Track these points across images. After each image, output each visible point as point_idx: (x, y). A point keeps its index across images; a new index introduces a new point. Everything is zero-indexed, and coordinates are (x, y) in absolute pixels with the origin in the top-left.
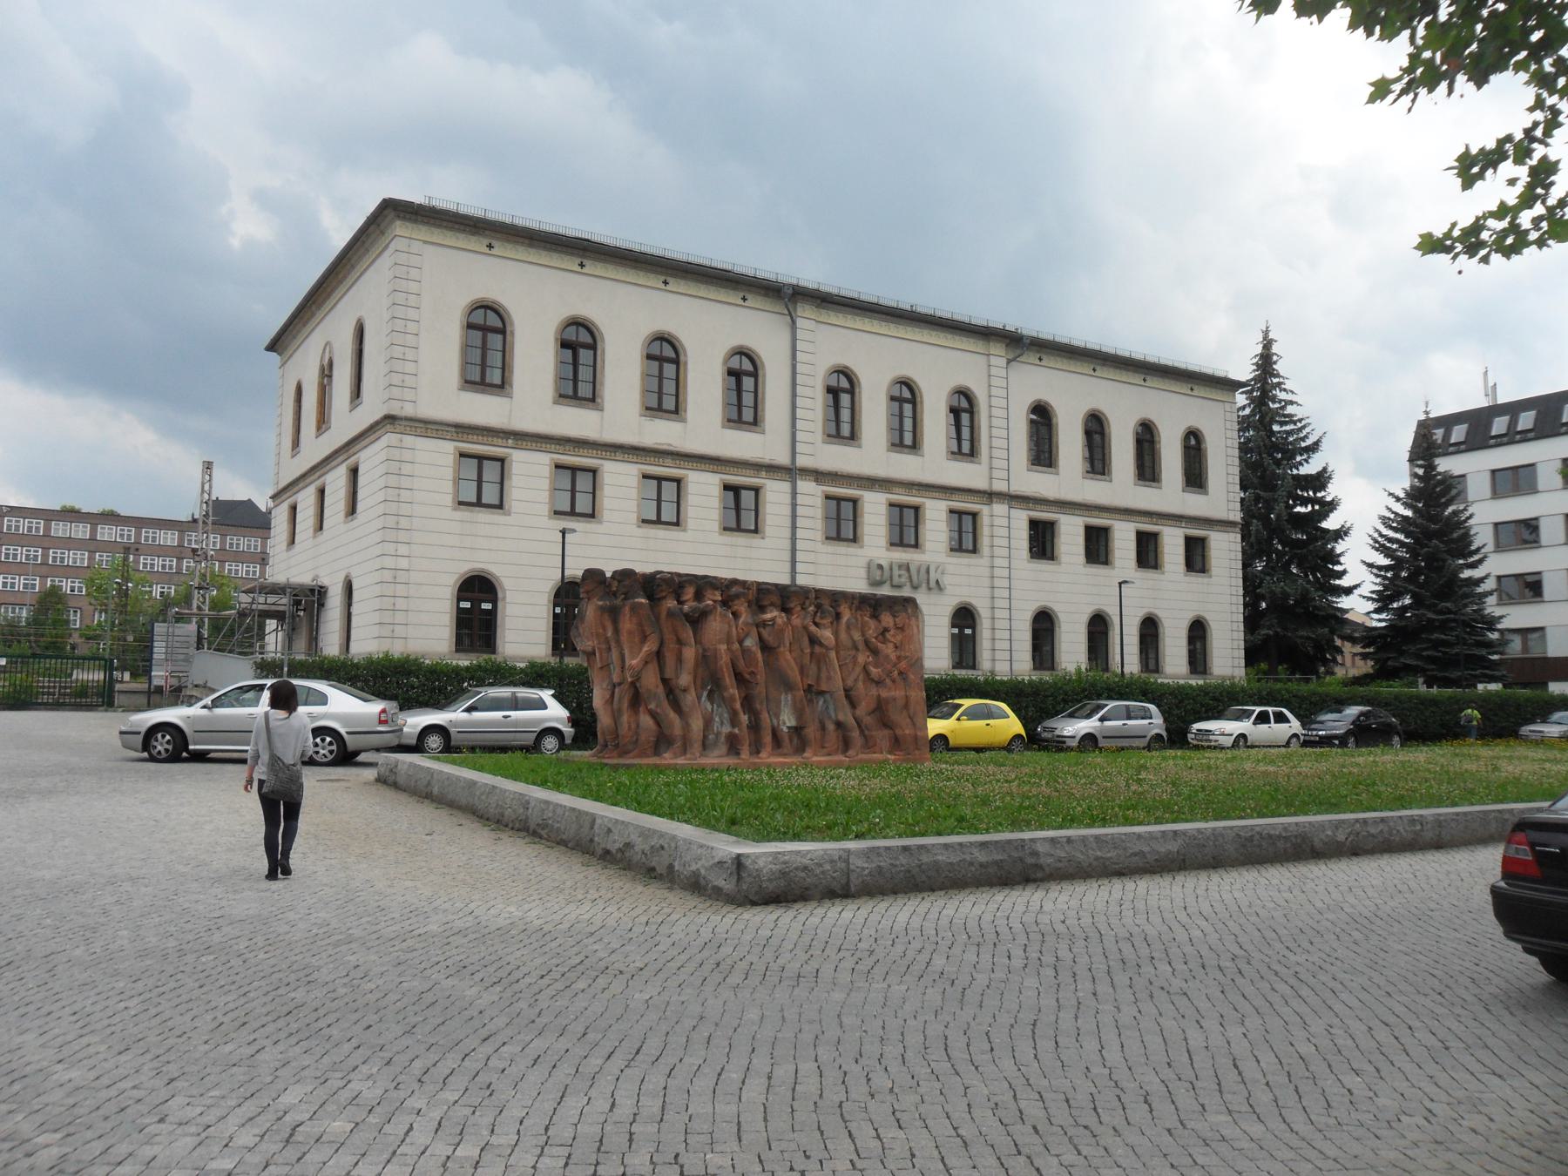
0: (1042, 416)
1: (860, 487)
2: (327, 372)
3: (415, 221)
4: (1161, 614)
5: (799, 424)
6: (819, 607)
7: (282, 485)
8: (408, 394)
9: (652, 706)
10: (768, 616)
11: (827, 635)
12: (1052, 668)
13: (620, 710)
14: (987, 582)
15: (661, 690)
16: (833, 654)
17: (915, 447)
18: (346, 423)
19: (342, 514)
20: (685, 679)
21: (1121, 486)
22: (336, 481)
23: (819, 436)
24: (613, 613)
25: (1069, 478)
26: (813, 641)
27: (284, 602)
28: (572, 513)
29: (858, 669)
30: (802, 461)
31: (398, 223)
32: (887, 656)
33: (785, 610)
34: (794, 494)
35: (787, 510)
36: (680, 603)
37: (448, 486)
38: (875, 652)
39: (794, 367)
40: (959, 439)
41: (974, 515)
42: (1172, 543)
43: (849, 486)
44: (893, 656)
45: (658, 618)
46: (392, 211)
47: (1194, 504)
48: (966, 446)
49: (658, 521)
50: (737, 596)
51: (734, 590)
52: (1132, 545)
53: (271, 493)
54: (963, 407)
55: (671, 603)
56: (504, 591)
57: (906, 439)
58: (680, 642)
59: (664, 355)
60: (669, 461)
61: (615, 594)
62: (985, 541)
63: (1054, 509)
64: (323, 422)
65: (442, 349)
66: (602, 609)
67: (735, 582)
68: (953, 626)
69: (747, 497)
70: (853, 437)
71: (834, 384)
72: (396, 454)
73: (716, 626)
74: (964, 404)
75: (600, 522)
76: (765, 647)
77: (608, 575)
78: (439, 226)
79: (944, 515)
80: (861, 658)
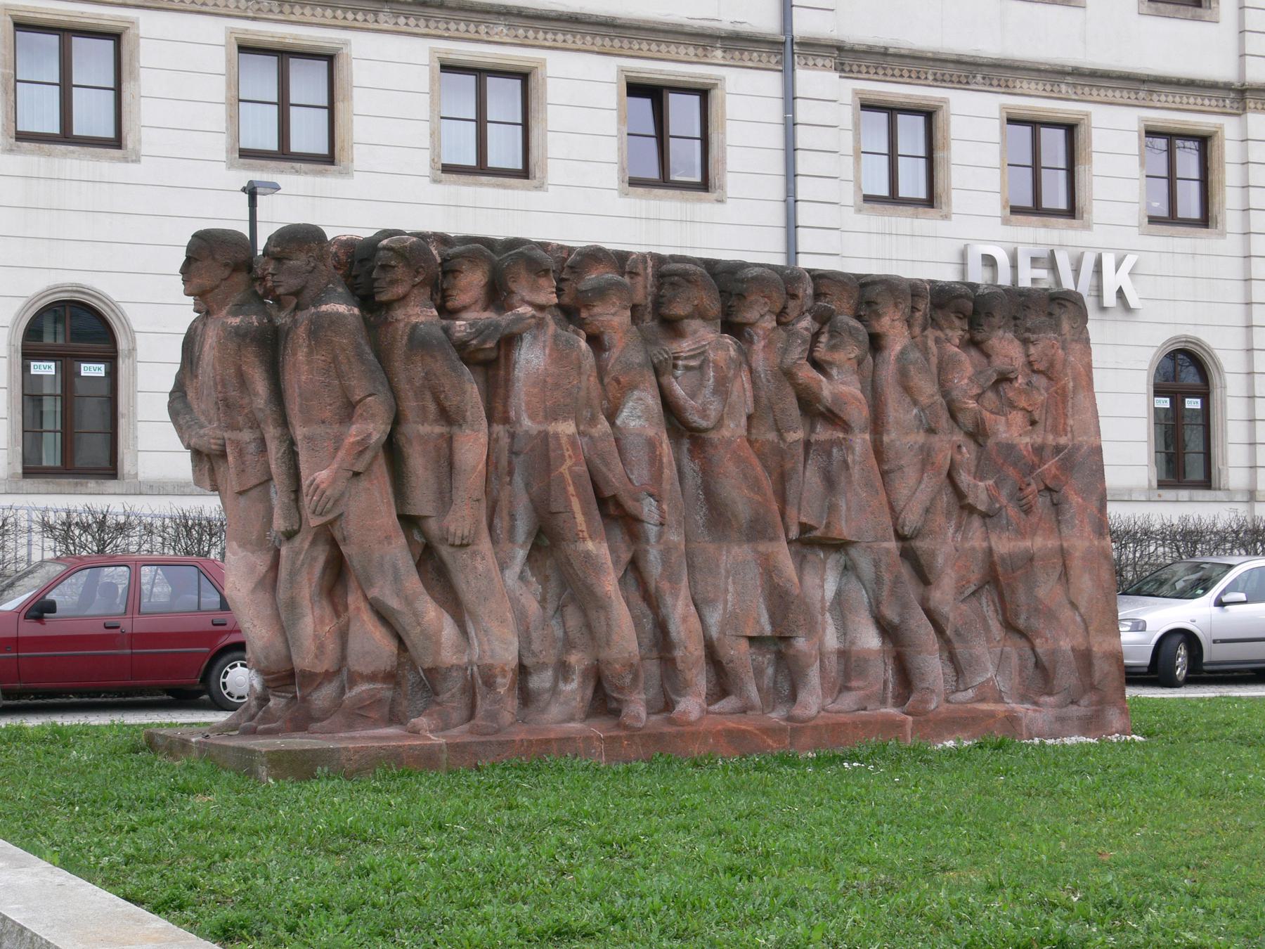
1: (940, 81)
6: (824, 319)
10: (685, 346)
13: (293, 604)
14: (1235, 292)
15: (399, 552)
20: (463, 518)
33: (733, 327)
34: (790, 98)
35: (775, 137)
36: (447, 312)
41: (1203, 142)
43: (898, 79)
45: (383, 357)
50: (601, 292)
51: (594, 277)
55: (419, 314)
56: (131, 334)
58: (448, 416)
60: (500, 30)
62: (1229, 199)
66: (240, 335)
67: (594, 256)
68: (1158, 392)
69: (682, 111)
75: (347, 173)
79: (1133, 142)
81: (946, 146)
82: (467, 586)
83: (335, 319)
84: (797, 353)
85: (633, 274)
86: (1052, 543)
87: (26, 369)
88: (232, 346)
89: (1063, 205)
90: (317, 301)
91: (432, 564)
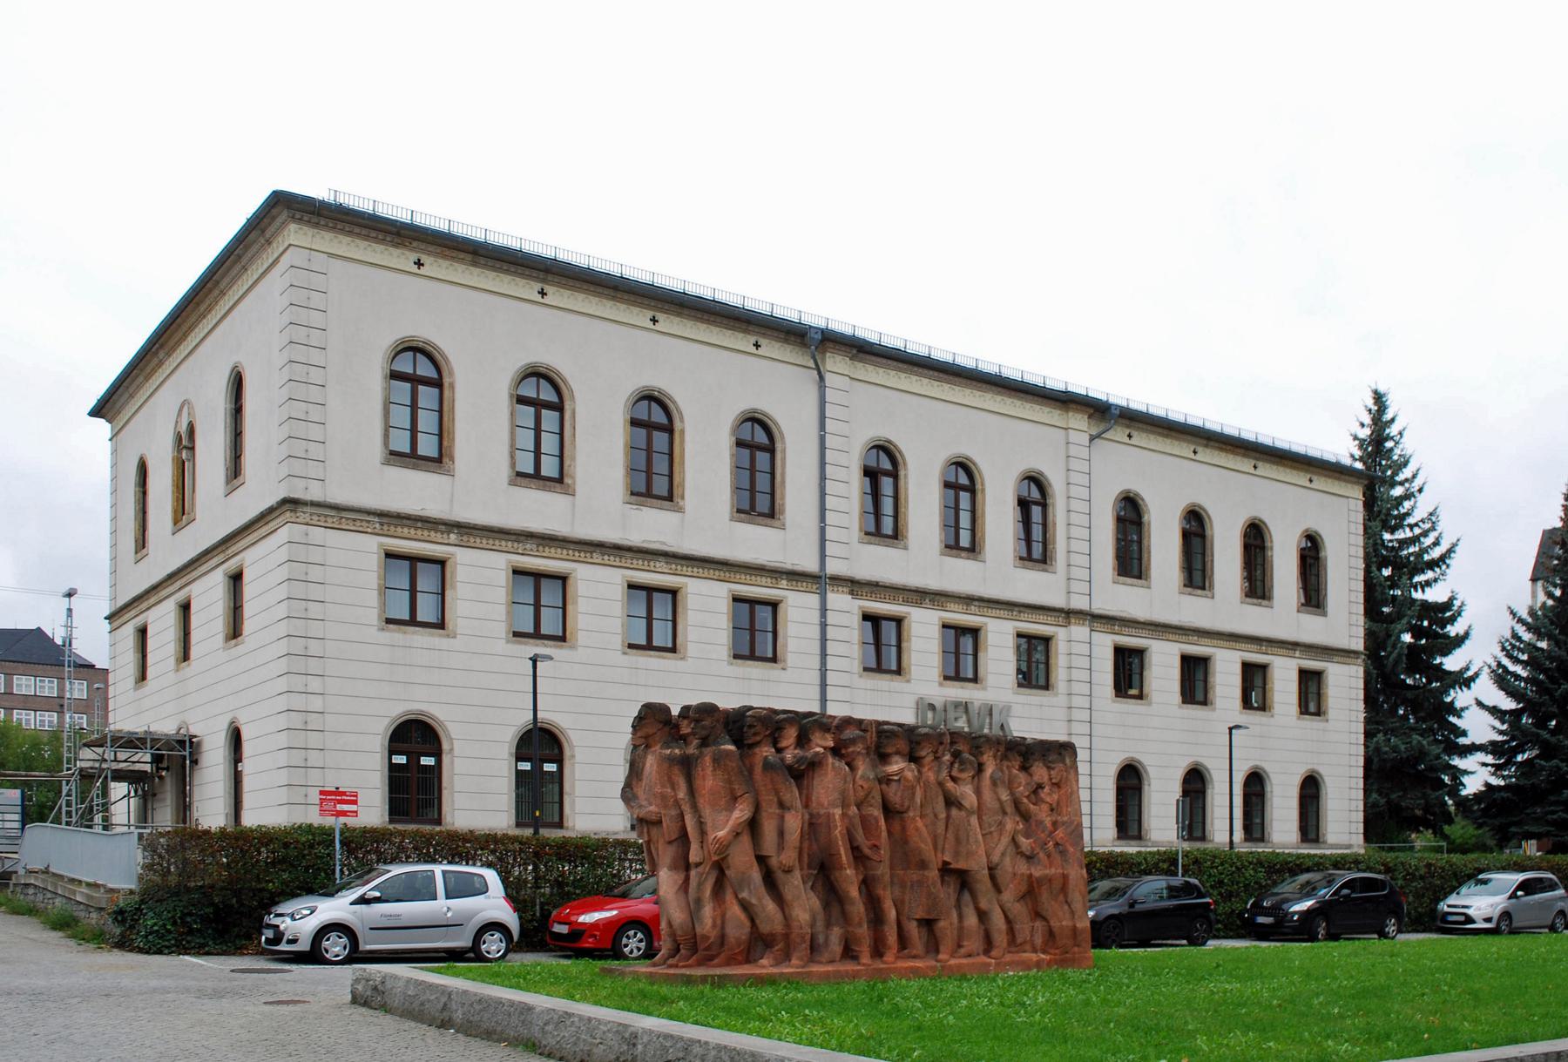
0: (1130, 514)
1: (906, 602)
2: (186, 443)
3: (316, 225)
4: (1269, 767)
5: (829, 516)
6: (956, 755)
7: (120, 603)
8: (314, 470)
9: (744, 895)
11: (966, 792)
12: (1139, 837)
13: (699, 901)
15: (756, 875)
16: (974, 820)
17: (974, 550)
18: (218, 511)
19: (221, 637)
21: (1224, 604)
22: (209, 593)
23: (855, 533)
24: (687, 765)
25: (1161, 593)
26: (951, 802)
27: (142, 760)
28: (537, 635)
29: (1005, 840)
30: (833, 567)
31: (293, 226)
32: (1040, 823)
33: (913, 758)
34: (824, 610)
36: (779, 750)
37: (373, 598)
38: (1025, 816)
39: (822, 440)
40: (1028, 540)
42: (1284, 676)
43: (893, 601)
44: (1048, 821)
45: (751, 771)
46: (283, 208)
47: (1311, 629)
48: (1036, 549)
49: (649, 646)
50: (853, 741)
52: (1237, 680)
53: (107, 613)
54: (1034, 499)
55: (767, 751)
57: (962, 540)
59: (654, 420)
60: (661, 565)
61: (684, 738)
62: (1060, 674)
63: (1144, 633)
64: (182, 511)
65: (360, 407)
66: (671, 760)
69: (888, 629)
70: (897, 536)
71: (873, 464)
72: (301, 553)
73: (828, 785)
74: (1035, 494)
76: (888, 810)
77: (675, 711)
78: (350, 233)
79: (1010, 641)
80: (1009, 826)
81: (909, 640)
82: (788, 893)
83: (728, 753)
84: (944, 773)
85: (865, 731)
86: (1060, 871)
87: (390, 759)
88: (666, 765)
89: (894, 667)
90: (716, 743)
91: (771, 882)
